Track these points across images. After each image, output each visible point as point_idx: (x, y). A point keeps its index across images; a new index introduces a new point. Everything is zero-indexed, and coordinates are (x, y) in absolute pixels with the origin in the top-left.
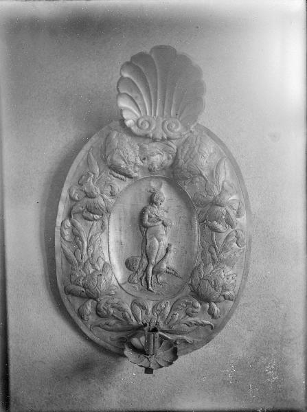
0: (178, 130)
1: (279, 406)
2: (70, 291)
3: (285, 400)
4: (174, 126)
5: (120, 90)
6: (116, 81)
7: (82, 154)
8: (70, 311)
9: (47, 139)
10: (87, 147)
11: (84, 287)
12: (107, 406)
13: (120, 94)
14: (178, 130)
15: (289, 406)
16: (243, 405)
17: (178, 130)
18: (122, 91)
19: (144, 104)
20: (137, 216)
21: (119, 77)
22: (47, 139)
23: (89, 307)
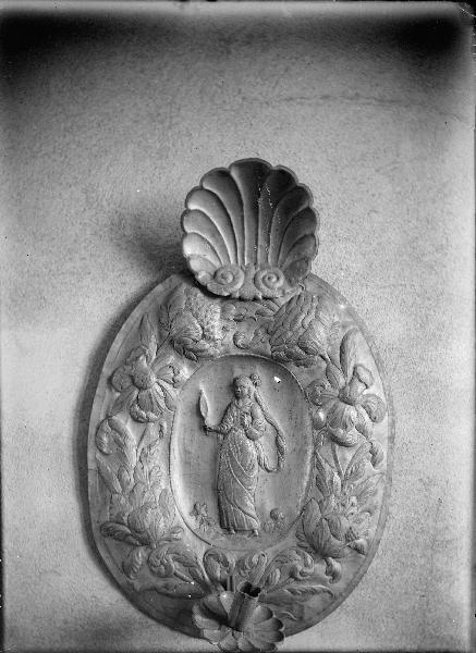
0: (278, 285)
1: (427, 645)
2: (112, 534)
3: (438, 637)
4: (274, 279)
5: (186, 227)
6: (183, 201)
7: (137, 313)
8: (109, 563)
9: (67, 221)
10: (145, 303)
11: (129, 527)
12: (156, 642)
13: (185, 234)
14: (278, 287)
15: (445, 647)
16: (373, 645)
17: (278, 285)
18: (188, 229)
19: (224, 246)
20: (195, 411)
21: (198, 184)
22: (67, 221)
23: (141, 555)
